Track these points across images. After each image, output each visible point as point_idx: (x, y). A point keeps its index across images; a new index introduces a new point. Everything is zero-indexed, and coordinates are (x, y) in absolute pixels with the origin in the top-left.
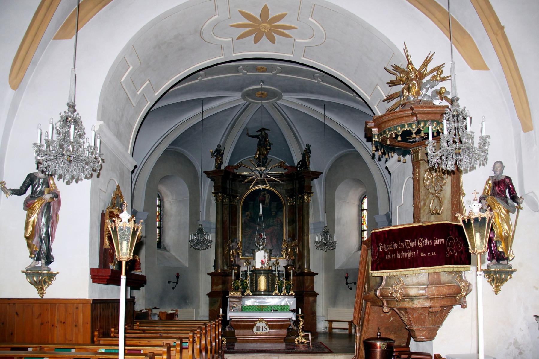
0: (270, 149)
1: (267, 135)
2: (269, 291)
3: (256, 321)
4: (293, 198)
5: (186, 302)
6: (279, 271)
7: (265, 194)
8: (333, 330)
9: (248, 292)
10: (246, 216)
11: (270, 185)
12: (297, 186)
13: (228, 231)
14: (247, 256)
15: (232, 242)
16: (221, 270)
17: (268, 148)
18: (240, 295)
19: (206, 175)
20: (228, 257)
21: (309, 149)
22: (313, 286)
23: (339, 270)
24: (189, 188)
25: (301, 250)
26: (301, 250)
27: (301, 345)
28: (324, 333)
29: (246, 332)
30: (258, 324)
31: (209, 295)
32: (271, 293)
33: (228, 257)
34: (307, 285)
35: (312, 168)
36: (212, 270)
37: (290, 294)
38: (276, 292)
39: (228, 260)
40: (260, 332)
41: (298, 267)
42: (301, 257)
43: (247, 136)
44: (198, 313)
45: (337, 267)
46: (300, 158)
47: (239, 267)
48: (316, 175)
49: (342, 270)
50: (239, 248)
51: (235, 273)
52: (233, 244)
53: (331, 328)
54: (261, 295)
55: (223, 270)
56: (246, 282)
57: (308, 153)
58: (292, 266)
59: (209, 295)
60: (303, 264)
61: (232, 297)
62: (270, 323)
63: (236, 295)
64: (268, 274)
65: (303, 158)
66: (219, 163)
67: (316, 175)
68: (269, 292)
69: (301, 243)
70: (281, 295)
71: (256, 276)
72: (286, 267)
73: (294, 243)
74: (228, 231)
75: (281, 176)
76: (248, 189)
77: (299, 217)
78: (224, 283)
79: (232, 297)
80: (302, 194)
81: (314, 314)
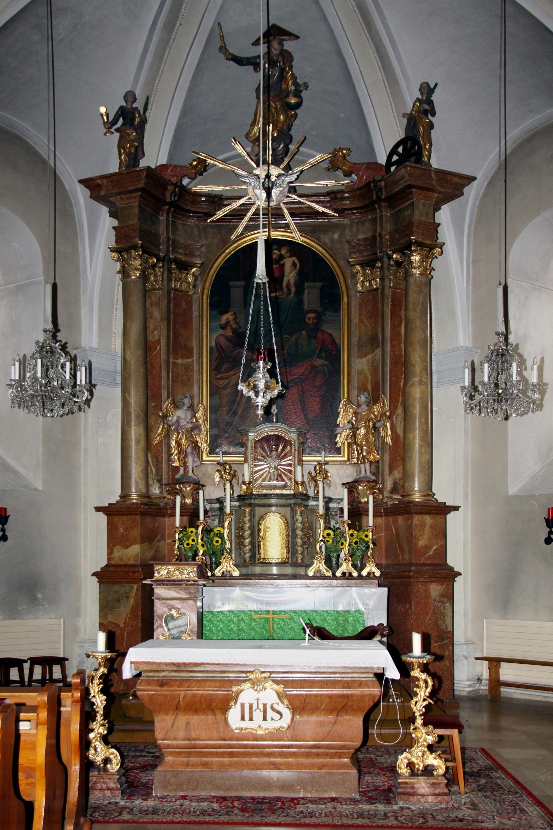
0: (298, 105)
1: (287, 57)
2: (295, 564)
3: (238, 682)
4: (373, 267)
5: (34, 599)
6: (328, 500)
7: (281, 257)
8: (503, 689)
9: (227, 566)
10: (223, 327)
11: (300, 228)
12: (388, 227)
13: (164, 374)
14: (225, 453)
15: (176, 406)
16: (140, 495)
17: (293, 101)
18: (193, 576)
19: (88, 192)
20: (165, 457)
21: (431, 103)
22: (444, 548)
23: (524, 498)
24: (41, 248)
25: (400, 431)
26: (400, 431)
27: (422, 785)
28: (474, 699)
29: (199, 726)
30: (247, 695)
31: (102, 576)
32: (301, 571)
33: (165, 457)
34: (422, 543)
35: (438, 160)
36: (113, 496)
37: (364, 573)
38: (319, 565)
39: (164, 466)
40: (257, 725)
41: (389, 485)
42: (399, 452)
43: (221, 56)
44: (76, 631)
45: (513, 489)
46: (398, 133)
47: (198, 486)
48: (452, 186)
49: (532, 497)
50: (197, 427)
51: (183, 505)
52: (179, 413)
53: (496, 683)
54: (271, 577)
55: (148, 496)
56: (221, 536)
57: (426, 112)
58: (373, 484)
59: (102, 576)
60: (407, 476)
61: (163, 583)
62: (295, 691)
63: (177, 576)
64: (292, 507)
65: (407, 130)
66: (133, 151)
67: (452, 186)
68: (295, 565)
69: (400, 410)
70: (334, 577)
71: (252, 515)
72: (351, 487)
73: (376, 408)
74: (164, 374)
75: (332, 197)
76: (226, 242)
77: (395, 328)
78: (150, 537)
79: (163, 583)
80: (405, 249)
81: (447, 637)
